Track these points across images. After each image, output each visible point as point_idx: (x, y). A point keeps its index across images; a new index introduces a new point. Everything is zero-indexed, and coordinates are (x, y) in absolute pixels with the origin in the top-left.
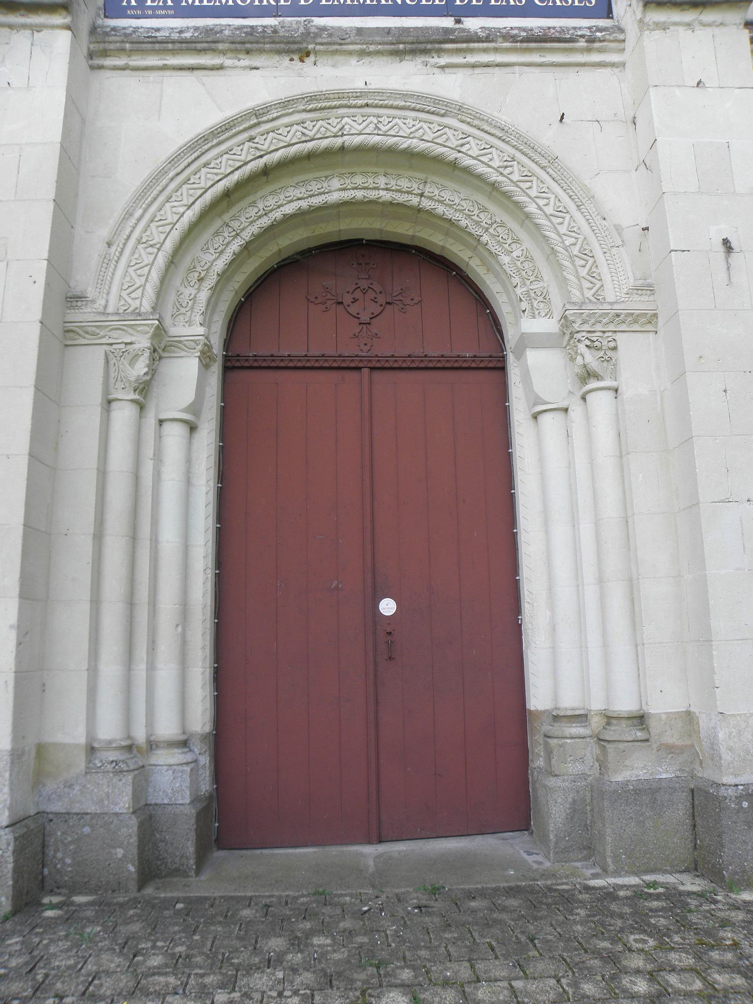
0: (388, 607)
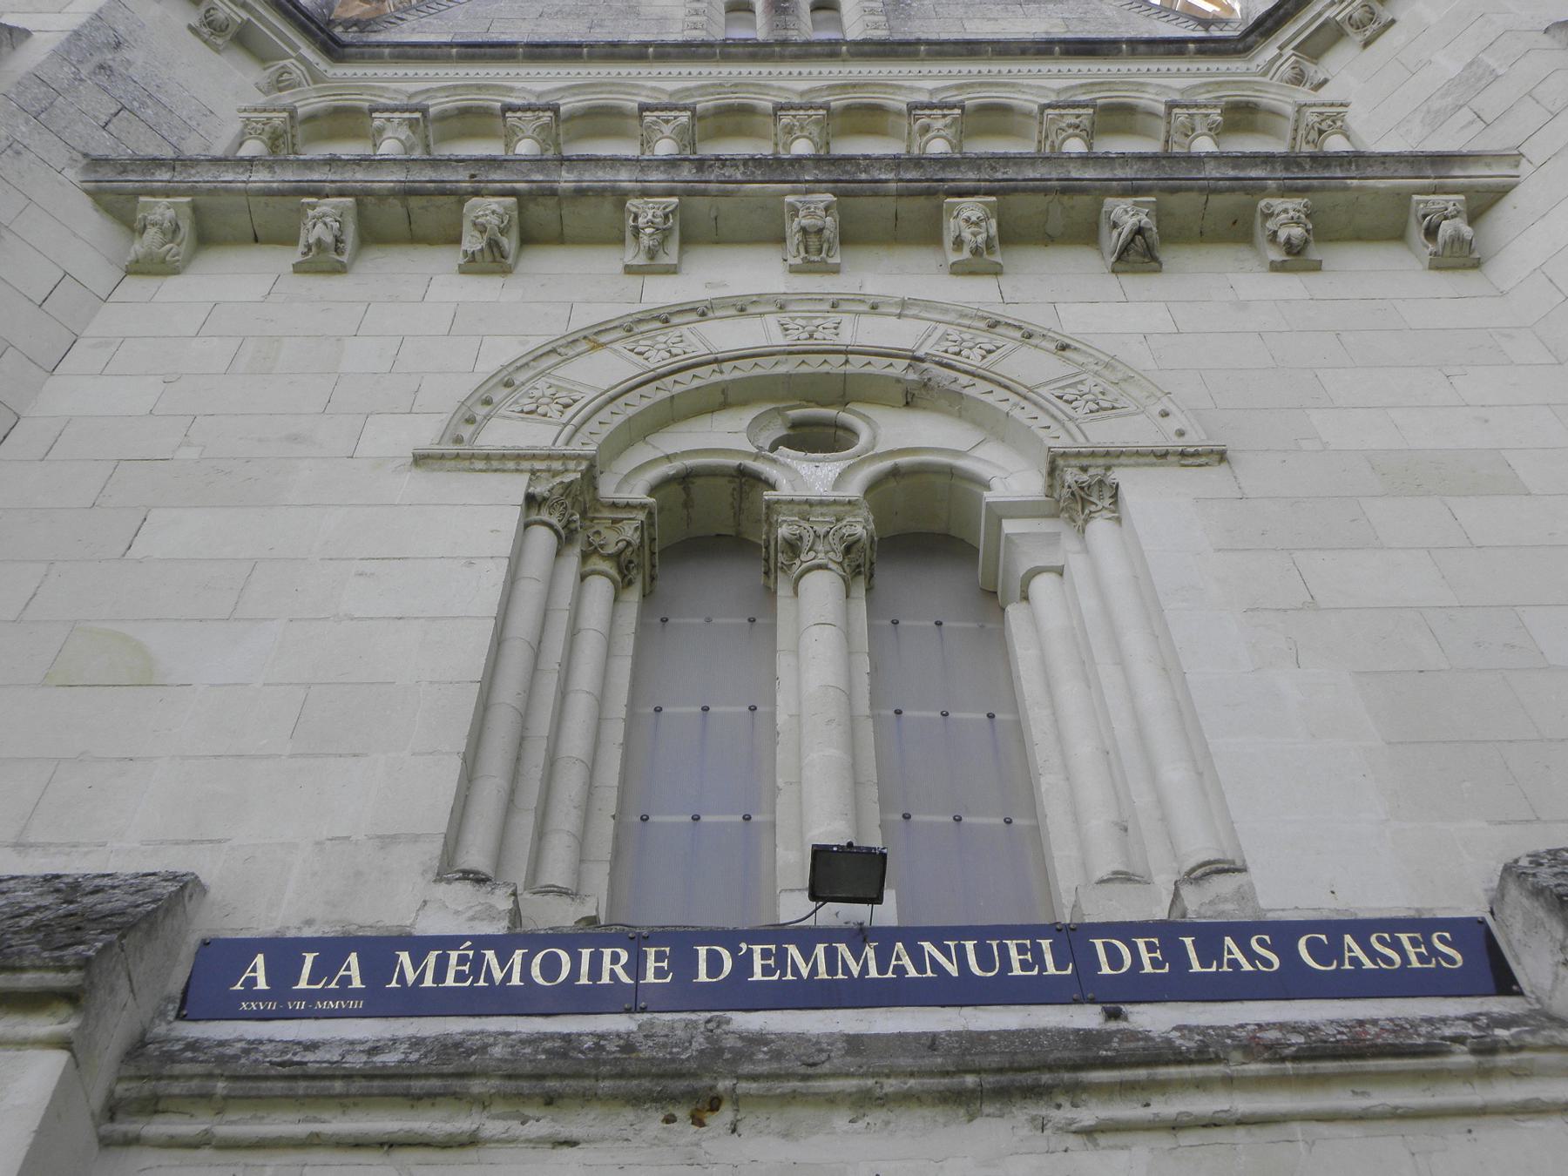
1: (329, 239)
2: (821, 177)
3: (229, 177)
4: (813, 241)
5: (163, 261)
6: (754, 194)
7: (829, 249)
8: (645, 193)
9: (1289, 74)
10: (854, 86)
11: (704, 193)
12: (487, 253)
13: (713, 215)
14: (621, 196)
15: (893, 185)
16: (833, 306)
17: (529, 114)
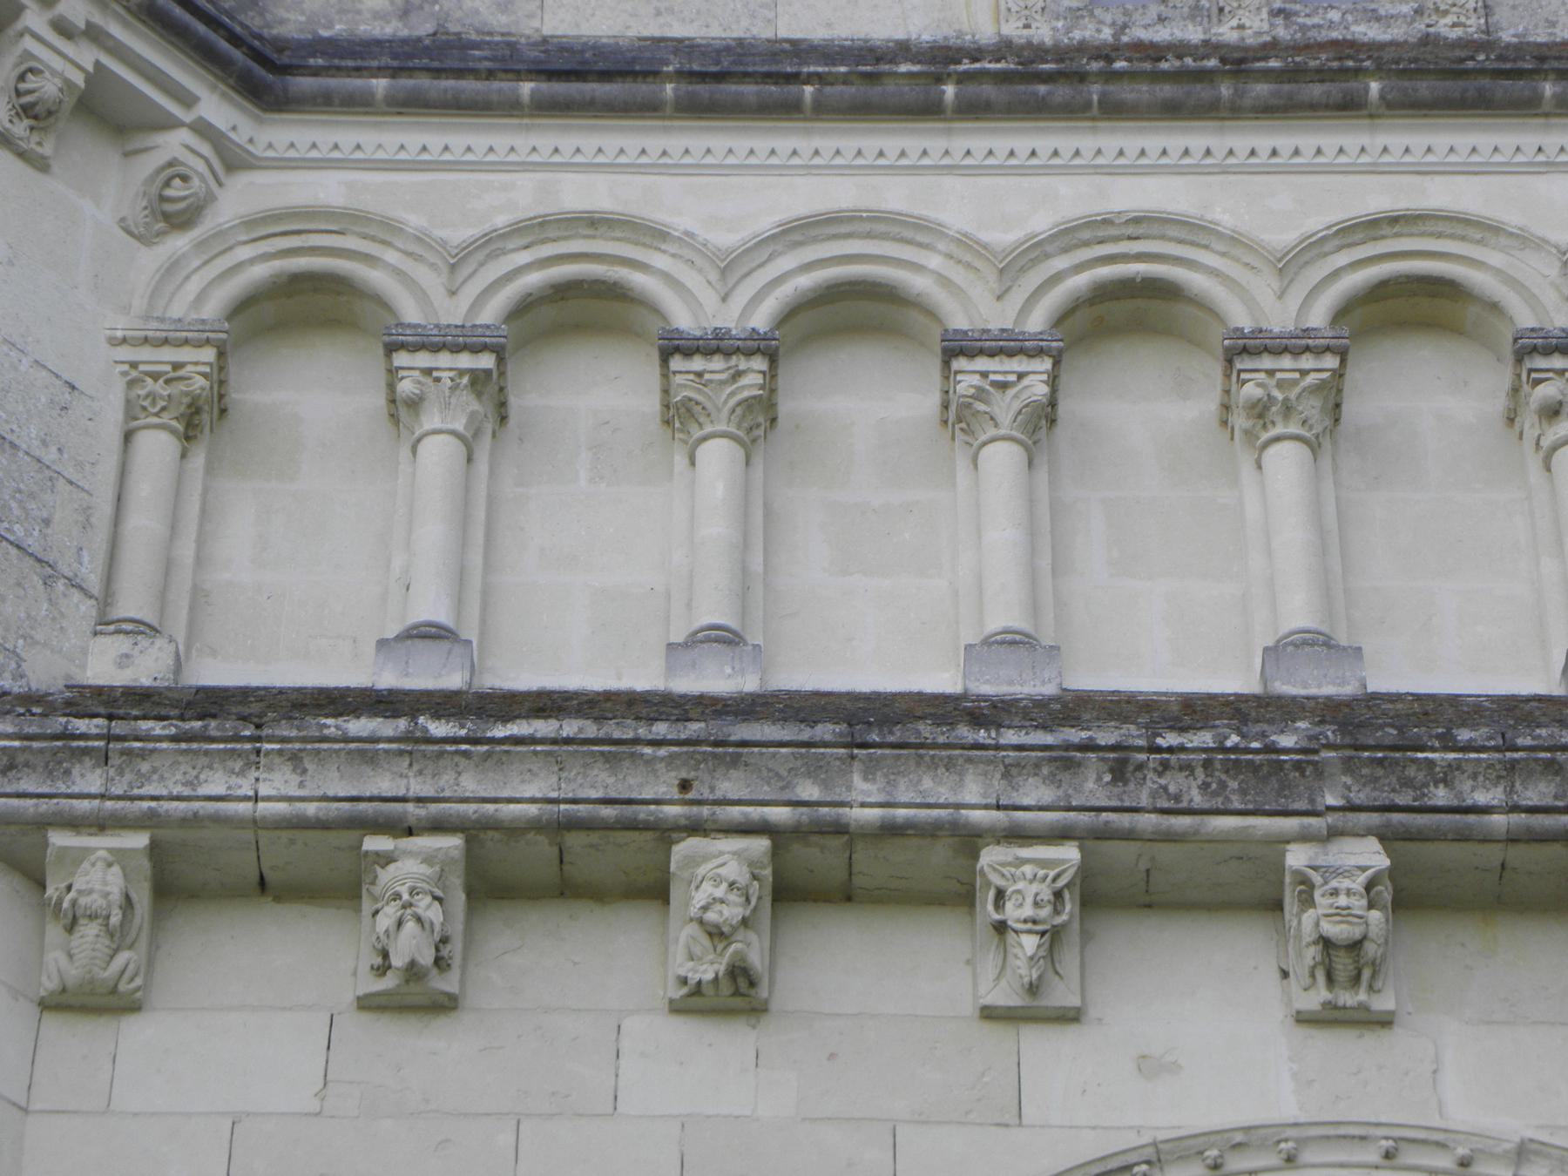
1: (426, 958)
2: (1359, 797)
3: (216, 784)
4: (1343, 964)
5: (114, 991)
6: (1225, 839)
7: (1374, 976)
8: (1017, 835)
10: (1394, 220)
11: (1129, 835)
12: (726, 987)
13: (1143, 866)
14: (970, 840)
15: (1498, 820)
16: (1388, 1155)
17: (717, 363)
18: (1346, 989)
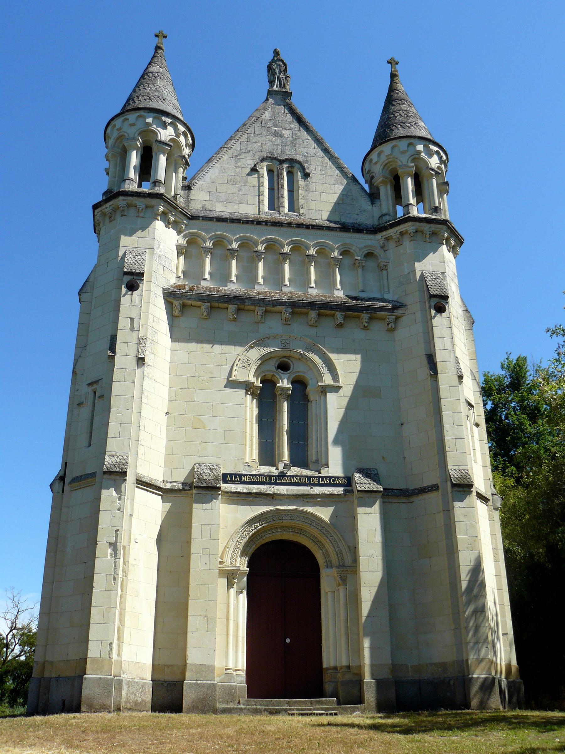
0: (288, 641)
9: (382, 245)
18: (287, 323)
